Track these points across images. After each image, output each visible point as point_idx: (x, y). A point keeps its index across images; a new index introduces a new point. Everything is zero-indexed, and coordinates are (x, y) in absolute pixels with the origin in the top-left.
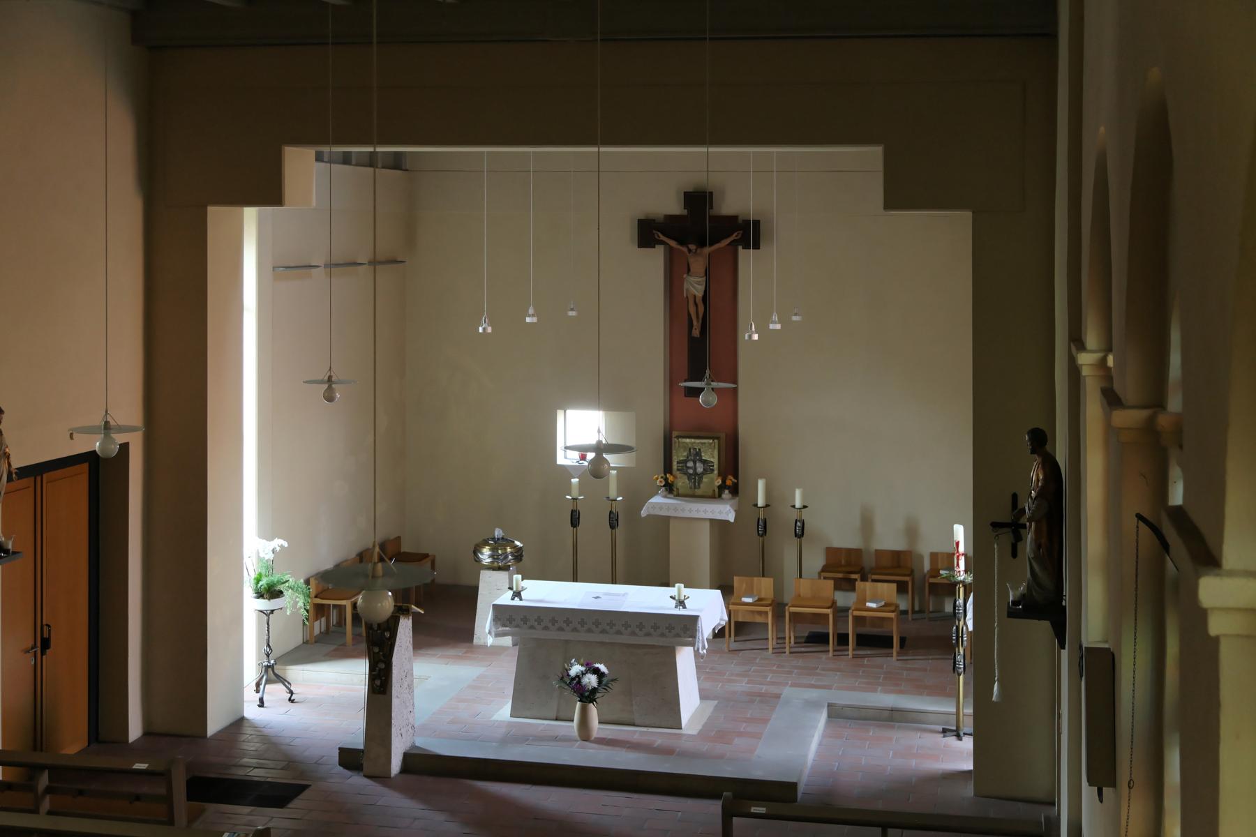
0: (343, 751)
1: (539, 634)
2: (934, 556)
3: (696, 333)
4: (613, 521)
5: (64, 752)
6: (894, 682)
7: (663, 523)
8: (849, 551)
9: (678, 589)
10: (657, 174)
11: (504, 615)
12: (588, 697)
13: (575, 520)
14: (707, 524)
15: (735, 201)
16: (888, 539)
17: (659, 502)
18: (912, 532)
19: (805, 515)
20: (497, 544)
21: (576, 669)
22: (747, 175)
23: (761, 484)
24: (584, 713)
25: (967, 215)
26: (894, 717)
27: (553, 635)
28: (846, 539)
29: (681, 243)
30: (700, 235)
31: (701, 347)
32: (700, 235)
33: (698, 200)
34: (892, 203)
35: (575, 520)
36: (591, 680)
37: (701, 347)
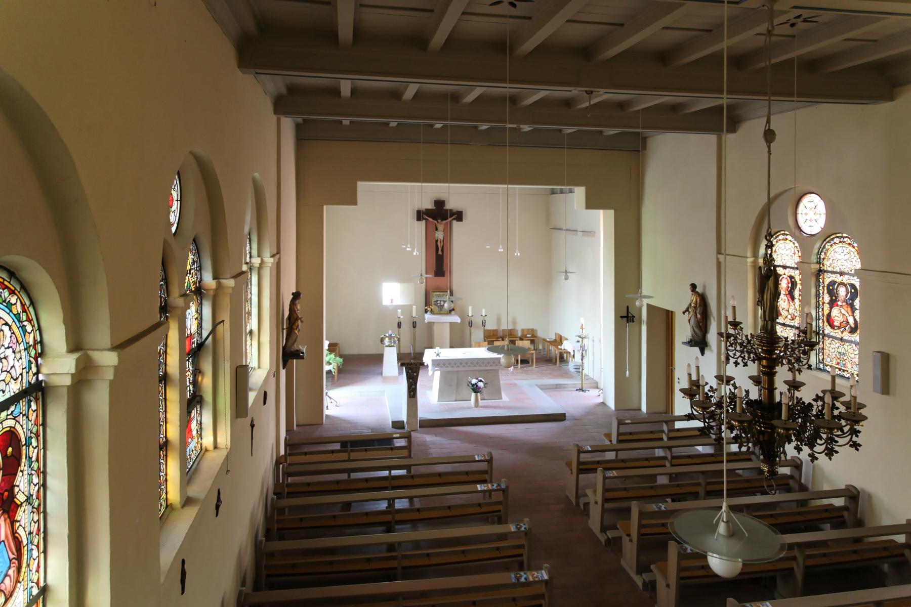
0: (393, 422)
1: (450, 369)
2: (523, 330)
3: (440, 253)
4: (414, 325)
5: (612, 404)
6: (555, 377)
7: (431, 325)
8: (493, 331)
9: (437, 349)
10: (424, 193)
11: (437, 363)
12: (476, 389)
13: (399, 325)
14: (448, 325)
15: (452, 205)
16: (504, 326)
17: (428, 317)
18: (514, 322)
19: (472, 319)
20: (390, 337)
21: (474, 381)
22: (455, 194)
23: (470, 308)
24: (476, 397)
25: (612, 211)
26: (557, 387)
27: (456, 369)
28: (490, 326)
29: (434, 219)
30: (438, 215)
31: (439, 263)
32: (438, 215)
33: (440, 204)
34: (355, 203)
35: (399, 325)
36: (481, 384)
37: (439, 263)
